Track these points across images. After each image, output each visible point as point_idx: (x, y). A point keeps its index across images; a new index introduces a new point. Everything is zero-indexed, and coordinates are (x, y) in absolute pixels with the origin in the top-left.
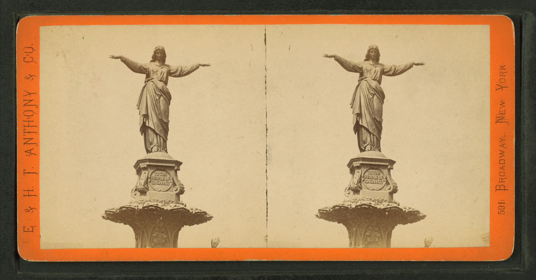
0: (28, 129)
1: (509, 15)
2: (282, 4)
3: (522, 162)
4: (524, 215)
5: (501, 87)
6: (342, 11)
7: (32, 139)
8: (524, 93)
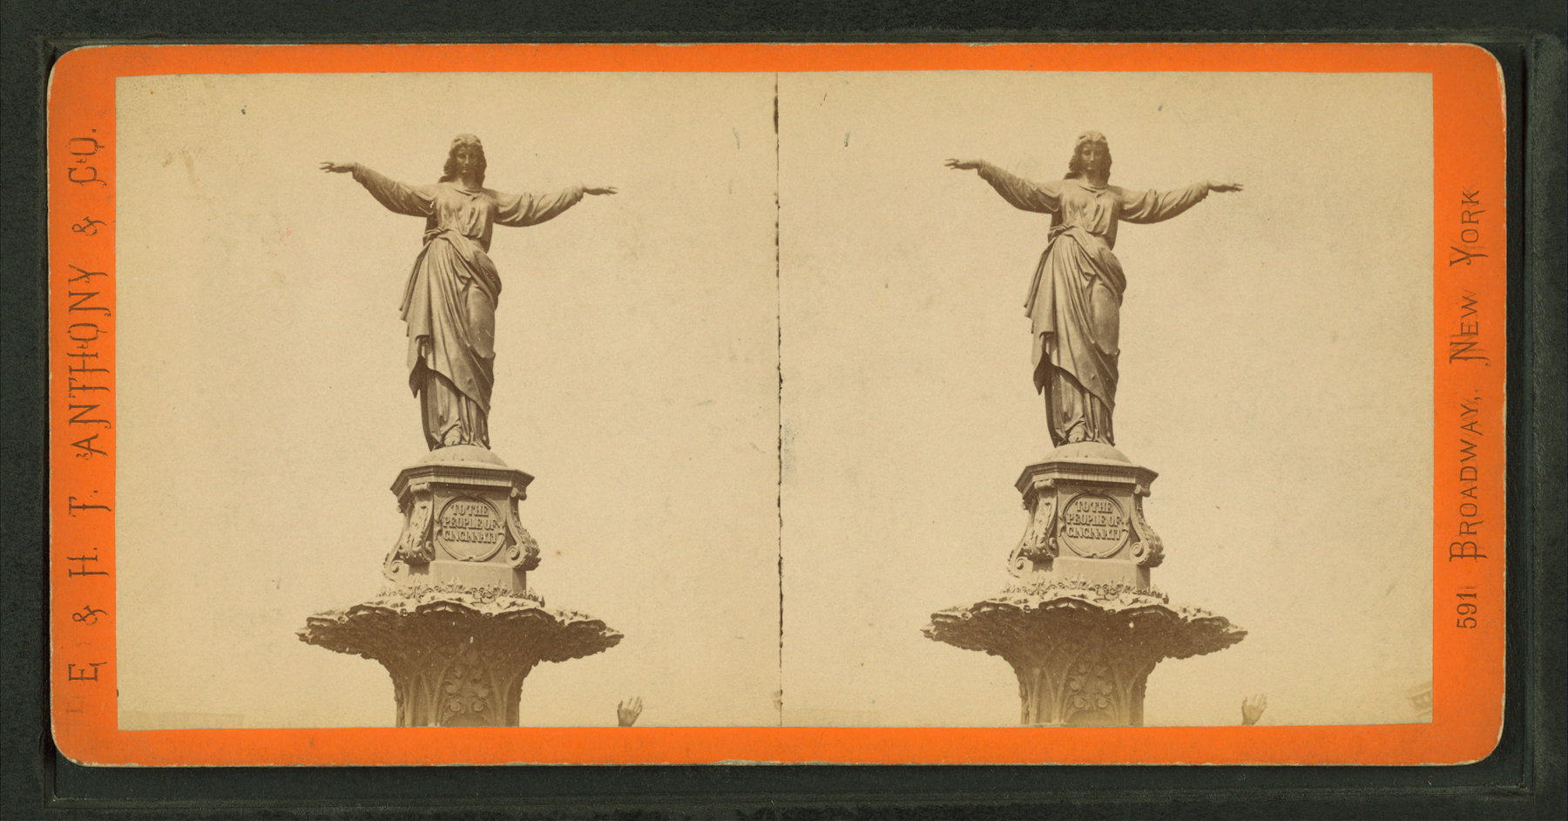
0: (82, 379)
1: (1489, 44)
2: (826, 13)
3: (1527, 475)
4: (1533, 631)
5: (1464, 256)
6: (999, 31)
7: (92, 407)
8: (1532, 274)
